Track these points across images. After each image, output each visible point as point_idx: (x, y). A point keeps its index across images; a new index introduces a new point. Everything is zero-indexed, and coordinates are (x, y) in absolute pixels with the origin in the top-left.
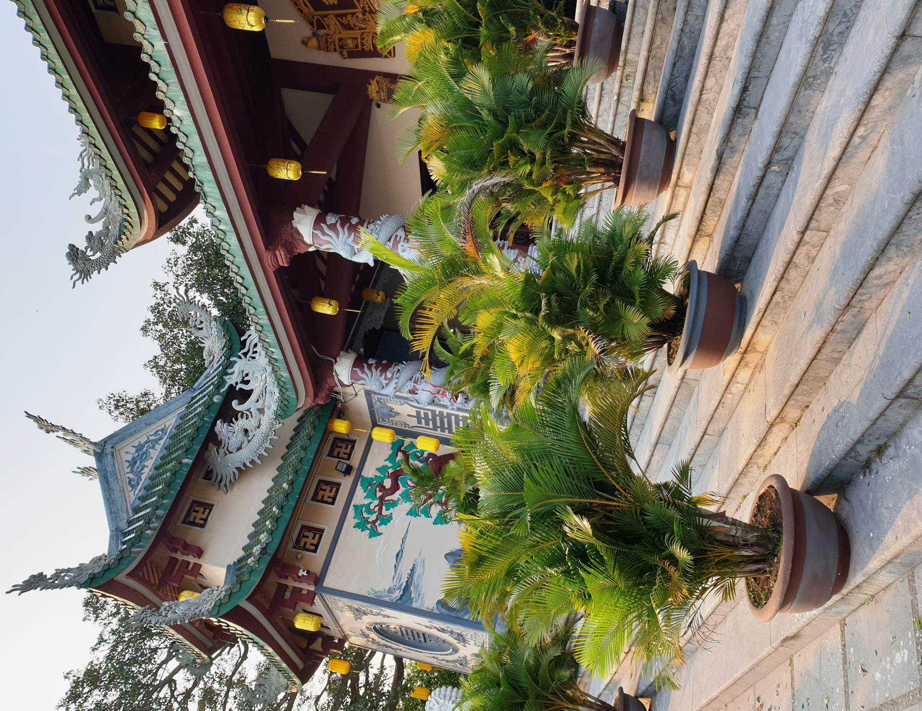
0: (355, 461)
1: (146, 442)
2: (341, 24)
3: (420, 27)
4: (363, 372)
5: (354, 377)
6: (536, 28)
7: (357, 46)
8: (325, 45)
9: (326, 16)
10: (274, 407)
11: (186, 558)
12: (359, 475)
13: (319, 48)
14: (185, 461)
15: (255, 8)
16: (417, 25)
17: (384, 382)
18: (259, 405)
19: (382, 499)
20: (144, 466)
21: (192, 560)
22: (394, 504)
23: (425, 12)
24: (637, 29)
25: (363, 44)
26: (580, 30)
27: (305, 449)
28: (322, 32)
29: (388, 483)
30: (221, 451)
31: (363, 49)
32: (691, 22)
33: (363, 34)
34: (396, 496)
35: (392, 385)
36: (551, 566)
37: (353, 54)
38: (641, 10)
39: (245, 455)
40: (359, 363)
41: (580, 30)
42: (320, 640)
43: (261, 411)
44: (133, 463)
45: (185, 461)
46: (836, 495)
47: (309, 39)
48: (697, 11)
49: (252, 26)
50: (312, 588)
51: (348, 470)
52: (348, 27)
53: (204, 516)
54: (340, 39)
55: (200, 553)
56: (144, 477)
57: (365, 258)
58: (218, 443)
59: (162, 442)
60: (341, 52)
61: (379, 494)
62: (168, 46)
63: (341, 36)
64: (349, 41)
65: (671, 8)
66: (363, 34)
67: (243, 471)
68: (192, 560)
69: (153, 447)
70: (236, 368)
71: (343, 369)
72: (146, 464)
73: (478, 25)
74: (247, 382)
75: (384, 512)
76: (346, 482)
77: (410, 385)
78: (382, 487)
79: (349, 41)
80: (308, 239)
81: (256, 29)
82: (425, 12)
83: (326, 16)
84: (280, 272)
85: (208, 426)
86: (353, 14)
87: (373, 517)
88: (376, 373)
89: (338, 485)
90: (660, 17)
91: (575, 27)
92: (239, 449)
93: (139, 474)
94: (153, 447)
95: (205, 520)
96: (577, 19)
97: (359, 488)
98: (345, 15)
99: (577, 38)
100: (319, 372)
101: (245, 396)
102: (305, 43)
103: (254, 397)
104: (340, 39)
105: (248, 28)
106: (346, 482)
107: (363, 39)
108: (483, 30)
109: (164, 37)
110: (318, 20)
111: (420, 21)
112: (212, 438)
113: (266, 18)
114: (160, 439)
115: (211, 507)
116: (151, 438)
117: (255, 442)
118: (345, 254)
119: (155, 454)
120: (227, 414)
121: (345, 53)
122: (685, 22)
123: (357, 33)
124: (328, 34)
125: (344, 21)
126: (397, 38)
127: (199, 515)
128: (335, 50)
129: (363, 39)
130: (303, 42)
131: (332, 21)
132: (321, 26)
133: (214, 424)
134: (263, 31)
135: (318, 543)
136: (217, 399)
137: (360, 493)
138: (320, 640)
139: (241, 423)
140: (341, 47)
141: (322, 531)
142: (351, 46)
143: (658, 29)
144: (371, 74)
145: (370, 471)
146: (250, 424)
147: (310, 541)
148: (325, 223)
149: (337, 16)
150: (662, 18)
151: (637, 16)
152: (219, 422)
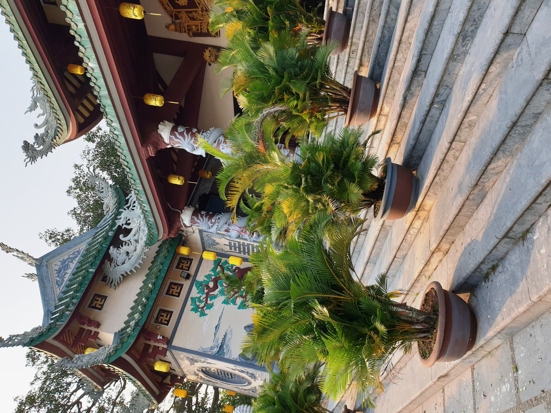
0: (192, 271)
1: (67, 259)
2: (189, 17)
3: (235, 20)
4: (198, 219)
5: (193, 221)
6: (301, 22)
7: (198, 30)
8: (179, 29)
9: (180, 12)
10: (145, 239)
11: (90, 328)
12: (194, 280)
13: (176, 30)
14: (91, 270)
15: (139, 6)
16: (232, 19)
17: (210, 225)
18: (136, 238)
19: (207, 294)
20: (66, 273)
21: (93, 329)
22: (215, 297)
23: (237, 12)
24: (358, 25)
25: (201, 29)
26: (326, 24)
27: (162, 264)
28: (177, 21)
29: (211, 285)
30: (113, 265)
31: (201, 32)
32: (389, 22)
33: (201, 23)
34: (216, 292)
35: (215, 227)
36: (305, 335)
37: (196, 35)
38: (361, 15)
39: (127, 267)
40: (195, 213)
41: (326, 24)
42: (169, 377)
43: (137, 241)
44: (59, 271)
45: (91, 270)
46: (469, 294)
47: (170, 25)
48: (393, 16)
49: (136, 16)
50: (165, 346)
51: (188, 277)
52: (193, 19)
53: (102, 303)
54: (188, 26)
55: (98, 325)
56: (65, 279)
57: (200, 152)
58: (111, 260)
59: (77, 259)
60: (189, 33)
61: (206, 291)
62: (86, 26)
63: (189, 24)
64: (194, 27)
65: (378, 14)
66: (201, 23)
67: (125, 277)
68: (93, 329)
69: (72, 262)
70: (123, 216)
71: (186, 217)
72: (67, 271)
73: (268, 20)
74: (129, 224)
75: (209, 302)
76: (186, 284)
77: (226, 227)
78: (208, 287)
79: (194, 27)
80: (167, 140)
81: (139, 18)
82: (237, 12)
83: (180, 12)
84: (150, 159)
85: (105, 249)
86: (196, 12)
87: (202, 305)
88: (206, 219)
89: (182, 285)
90: (371, 18)
91: (323, 23)
92: (123, 263)
93: (63, 278)
94: (72, 262)
95: (102, 306)
96: (325, 18)
97: (194, 287)
98: (191, 12)
99: (324, 29)
100: (171, 218)
101: (127, 232)
102: (167, 27)
103: (133, 233)
104: (188, 26)
105: (134, 17)
106: (186, 284)
107: (201, 26)
108: (270, 23)
109: (84, 21)
110: (175, 14)
111: (235, 16)
112: (107, 257)
113: (144, 12)
114: (76, 257)
115: (105, 298)
116: (71, 256)
117: (133, 259)
118: (188, 150)
119: (73, 266)
120: (116, 243)
121: (191, 34)
122: (386, 22)
123: (198, 23)
124: (181, 23)
125: (191, 15)
126: (221, 25)
127: (99, 303)
128: (185, 32)
129: (201, 26)
130: (166, 27)
131: (184, 15)
132: (177, 18)
133: (109, 249)
134: (142, 20)
135: (169, 320)
136: (111, 234)
137: (194, 289)
138: (169, 377)
139: (125, 248)
140: (189, 30)
141: (172, 312)
142: (195, 29)
143: (370, 25)
144: (206, 46)
145: (200, 278)
146: (130, 248)
147: (164, 318)
148: (177, 131)
149: (187, 12)
150: (373, 19)
151: (359, 18)
152: (111, 247)
